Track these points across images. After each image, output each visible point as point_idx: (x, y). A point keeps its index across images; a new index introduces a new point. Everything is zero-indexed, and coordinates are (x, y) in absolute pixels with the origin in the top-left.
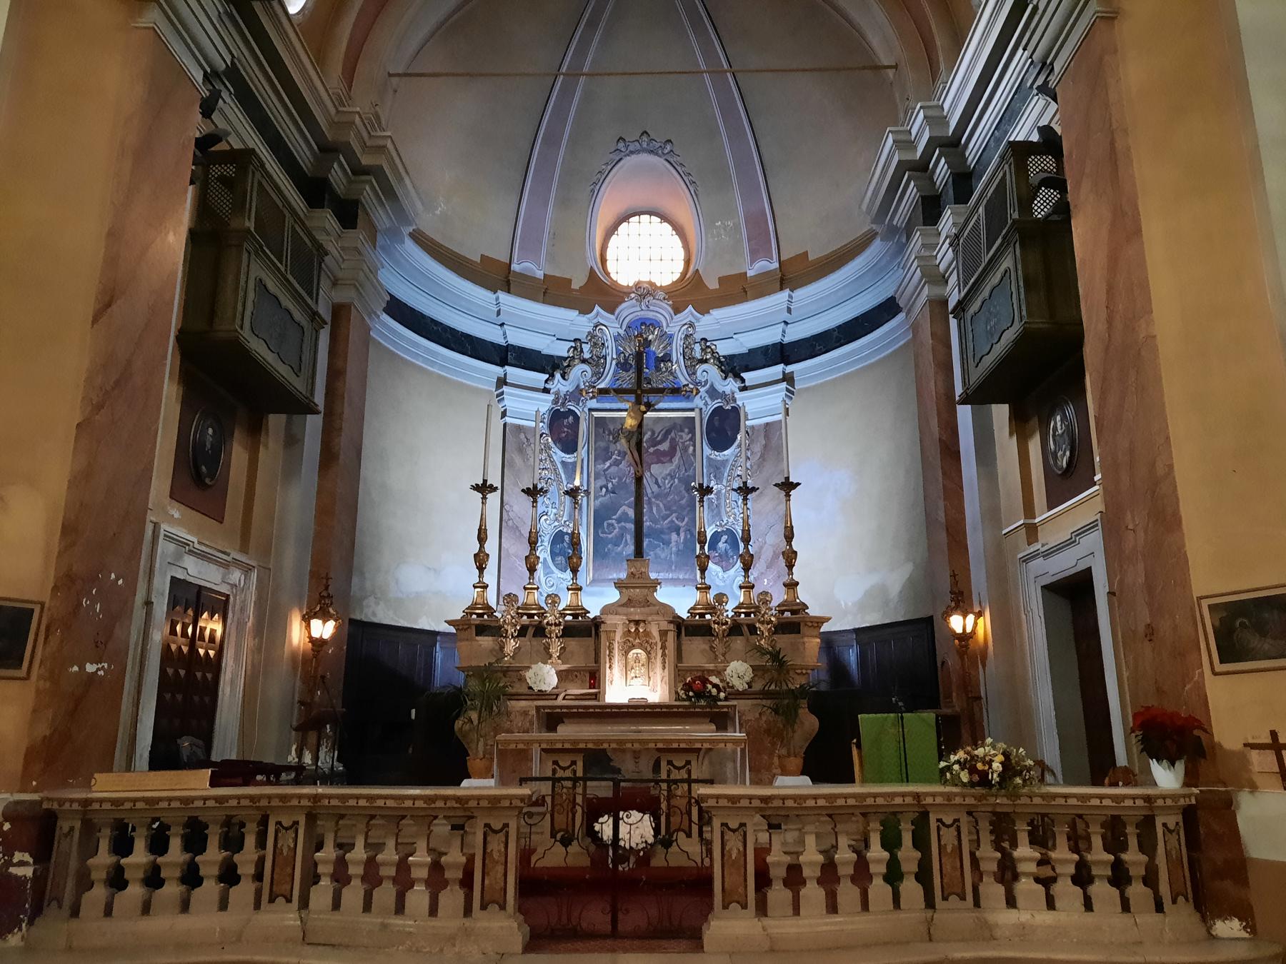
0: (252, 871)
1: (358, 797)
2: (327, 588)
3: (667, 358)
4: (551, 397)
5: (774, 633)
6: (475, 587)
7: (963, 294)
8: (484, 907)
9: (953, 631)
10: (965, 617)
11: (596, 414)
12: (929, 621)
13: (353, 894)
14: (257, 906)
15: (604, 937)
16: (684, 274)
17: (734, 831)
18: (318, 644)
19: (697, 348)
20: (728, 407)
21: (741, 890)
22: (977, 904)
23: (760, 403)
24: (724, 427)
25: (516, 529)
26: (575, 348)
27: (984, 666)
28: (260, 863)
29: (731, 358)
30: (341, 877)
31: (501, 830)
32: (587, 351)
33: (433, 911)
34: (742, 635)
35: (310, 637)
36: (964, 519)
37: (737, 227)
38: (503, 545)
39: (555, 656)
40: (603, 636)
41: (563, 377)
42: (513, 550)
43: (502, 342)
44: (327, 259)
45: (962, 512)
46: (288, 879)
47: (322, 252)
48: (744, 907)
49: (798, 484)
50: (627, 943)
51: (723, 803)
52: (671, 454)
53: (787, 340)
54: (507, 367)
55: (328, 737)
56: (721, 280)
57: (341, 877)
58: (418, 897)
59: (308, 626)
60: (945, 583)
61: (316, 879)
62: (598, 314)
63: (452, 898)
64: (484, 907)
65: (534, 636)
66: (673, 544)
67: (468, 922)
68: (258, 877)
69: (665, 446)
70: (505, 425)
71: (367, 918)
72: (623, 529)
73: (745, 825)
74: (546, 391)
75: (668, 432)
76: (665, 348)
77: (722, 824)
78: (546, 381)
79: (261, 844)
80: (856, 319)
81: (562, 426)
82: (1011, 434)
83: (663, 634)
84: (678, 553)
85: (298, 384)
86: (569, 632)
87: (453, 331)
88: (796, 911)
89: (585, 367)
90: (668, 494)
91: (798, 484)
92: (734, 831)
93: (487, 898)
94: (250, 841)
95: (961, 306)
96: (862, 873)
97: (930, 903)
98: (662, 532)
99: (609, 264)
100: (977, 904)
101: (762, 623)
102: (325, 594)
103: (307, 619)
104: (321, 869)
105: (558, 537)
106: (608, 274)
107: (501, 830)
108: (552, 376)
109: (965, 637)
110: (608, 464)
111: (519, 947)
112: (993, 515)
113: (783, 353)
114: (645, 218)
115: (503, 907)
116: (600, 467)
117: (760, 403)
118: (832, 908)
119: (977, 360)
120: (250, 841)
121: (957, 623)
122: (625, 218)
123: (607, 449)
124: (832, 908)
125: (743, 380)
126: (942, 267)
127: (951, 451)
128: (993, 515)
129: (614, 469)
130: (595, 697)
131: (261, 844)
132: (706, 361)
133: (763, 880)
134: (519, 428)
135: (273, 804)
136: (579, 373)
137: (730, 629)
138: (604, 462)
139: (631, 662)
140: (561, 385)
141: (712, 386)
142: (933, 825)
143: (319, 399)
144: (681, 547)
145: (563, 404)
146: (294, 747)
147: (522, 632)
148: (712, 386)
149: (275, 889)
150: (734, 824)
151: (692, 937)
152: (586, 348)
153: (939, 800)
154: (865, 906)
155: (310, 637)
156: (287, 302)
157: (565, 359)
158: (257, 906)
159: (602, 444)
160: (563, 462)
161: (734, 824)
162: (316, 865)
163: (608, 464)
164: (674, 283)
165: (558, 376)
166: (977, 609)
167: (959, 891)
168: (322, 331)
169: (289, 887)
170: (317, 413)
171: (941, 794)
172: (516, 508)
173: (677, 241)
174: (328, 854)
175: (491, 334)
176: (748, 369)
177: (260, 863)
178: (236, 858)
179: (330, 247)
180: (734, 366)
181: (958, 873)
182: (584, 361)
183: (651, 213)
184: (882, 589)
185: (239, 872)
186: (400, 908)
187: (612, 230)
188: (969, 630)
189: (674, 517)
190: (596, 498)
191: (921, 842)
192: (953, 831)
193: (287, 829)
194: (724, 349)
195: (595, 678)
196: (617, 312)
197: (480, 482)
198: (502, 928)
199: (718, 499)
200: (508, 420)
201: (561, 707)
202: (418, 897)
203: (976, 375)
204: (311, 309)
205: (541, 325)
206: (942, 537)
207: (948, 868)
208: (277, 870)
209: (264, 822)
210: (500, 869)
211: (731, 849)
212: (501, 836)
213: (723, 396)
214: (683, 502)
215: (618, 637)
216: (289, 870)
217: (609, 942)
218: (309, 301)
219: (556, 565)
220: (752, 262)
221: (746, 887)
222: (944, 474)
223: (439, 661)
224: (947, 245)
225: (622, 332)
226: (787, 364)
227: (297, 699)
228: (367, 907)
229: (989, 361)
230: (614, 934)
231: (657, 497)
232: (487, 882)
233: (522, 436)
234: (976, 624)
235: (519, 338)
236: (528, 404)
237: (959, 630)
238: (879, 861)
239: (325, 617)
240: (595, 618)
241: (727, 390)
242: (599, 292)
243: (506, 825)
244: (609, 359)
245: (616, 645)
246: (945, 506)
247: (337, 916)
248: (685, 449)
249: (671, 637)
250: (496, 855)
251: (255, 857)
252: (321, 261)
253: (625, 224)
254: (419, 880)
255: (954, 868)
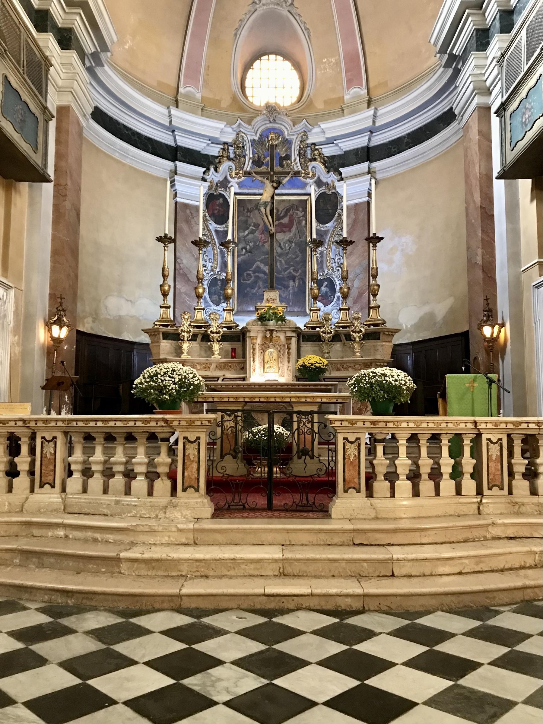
0: (27, 468)
1: (96, 420)
2: (61, 304)
3: (288, 157)
4: (207, 184)
5: (362, 340)
6: (161, 307)
7: (505, 98)
8: (184, 490)
9: (485, 336)
10: (493, 327)
11: (239, 197)
12: (466, 335)
13: (96, 482)
14: (32, 491)
15: (263, 510)
16: (300, 99)
17: (352, 443)
18: (57, 341)
19: (309, 151)
20: (330, 193)
21: (356, 480)
22: (510, 493)
23: (351, 188)
24: (328, 204)
25: (185, 275)
26: (224, 149)
27: (503, 361)
28: (32, 463)
29: (332, 158)
30: (87, 473)
31: (195, 442)
32: (233, 151)
33: (150, 493)
34: (341, 341)
35: (52, 337)
36: (494, 262)
37: (338, 63)
38: (177, 286)
39: (216, 353)
40: (248, 342)
41: (216, 171)
42: (183, 290)
43: (173, 144)
44: (51, 69)
45: (493, 257)
46: (52, 473)
47: (48, 64)
48: (358, 491)
49: (382, 238)
50: (279, 514)
51: (345, 424)
52: (289, 227)
53: (372, 144)
54: (177, 163)
55: (67, 404)
56: (326, 102)
57: (87, 473)
58: (140, 484)
59: (50, 330)
60: (480, 302)
61: (70, 474)
62: (240, 124)
63: (162, 485)
64: (184, 490)
65: (202, 341)
66: (291, 288)
67: (174, 500)
68: (31, 473)
69: (285, 221)
70: (176, 203)
71: (105, 497)
72: (257, 278)
73: (359, 439)
74: (204, 180)
75: (288, 210)
76: (286, 150)
77: (344, 439)
78: (204, 173)
79: (32, 451)
80: (420, 128)
81: (216, 205)
82: (532, 200)
83: (289, 339)
84: (294, 294)
85: (36, 159)
86: (224, 338)
87: (139, 135)
88: (393, 495)
89: (231, 163)
90: (288, 254)
91: (382, 238)
92: (352, 443)
93: (186, 484)
94: (24, 449)
95: (503, 107)
96: (435, 475)
97: (480, 492)
98: (283, 279)
99: (247, 90)
100: (510, 493)
101: (355, 332)
102: (60, 308)
103: (48, 325)
104: (73, 467)
105: (213, 282)
106: (246, 97)
107: (195, 442)
108: (208, 169)
109: (494, 340)
110: (246, 232)
111: (209, 516)
112: (514, 257)
113: (368, 154)
114: (272, 57)
115: (197, 490)
116: (241, 234)
117: (351, 188)
118: (416, 493)
119: (513, 145)
120: (24, 449)
121: (487, 331)
122: (257, 56)
123: (246, 222)
124: (416, 493)
125: (340, 174)
126: (488, 83)
127: (487, 216)
128: (514, 257)
129: (251, 236)
130: (244, 379)
131: (32, 451)
132: (315, 160)
133: (371, 478)
134: (186, 206)
135: (38, 425)
136: (225, 165)
137: (333, 337)
138: (244, 231)
139: (267, 358)
140: (214, 177)
141: (319, 178)
142: (484, 442)
143: (51, 171)
144: (296, 290)
145: (216, 190)
146: (45, 409)
147: (194, 338)
148: (319, 178)
149: (43, 479)
150: (352, 438)
151: (324, 512)
152: (231, 149)
153: (489, 426)
154: (437, 493)
155: (52, 337)
156: (25, 96)
157: (217, 157)
158: (32, 491)
159: (243, 218)
160: (216, 231)
161: (352, 438)
162: (69, 465)
163: (246, 232)
164: (292, 105)
165: (212, 169)
166: (500, 322)
167: (499, 484)
168: (51, 122)
169: (51, 478)
170: (49, 181)
171: (491, 422)
172: (185, 261)
173: (294, 74)
174: (78, 455)
175: (166, 138)
176: (344, 166)
177: (32, 463)
178: (16, 459)
179: (53, 62)
180: (335, 164)
181: (500, 472)
182: (229, 159)
183: (276, 54)
184: (431, 316)
185: (18, 469)
186: (128, 492)
187: (248, 66)
188: (495, 335)
189: (291, 270)
190: (238, 256)
191: (476, 452)
192: (497, 446)
193: (49, 441)
194: (328, 151)
195: (243, 368)
196: (253, 124)
197: (163, 235)
198: (197, 503)
199: (322, 257)
200: (178, 199)
201: (221, 385)
202: (140, 484)
203: (511, 157)
204: (42, 105)
205: (202, 130)
206: (479, 274)
207: (492, 470)
208: (43, 467)
209: (33, 437)
210: (195, 466)
211: (349, 456)
212: (195, 445)
213: (327, 184)
214: (298, 259)
215: (259, 341)
216: (52, 467)
217: (267, 513)
218: (40, 98)
219: (212, 301)
220: (348, 89)
221: (359, 478)
222: (483, 231)
223: (136, 362)
224: (494, 63)
225: (256, 138)
226: (371, 161)
227: (45, 378)
228: (105, 491)
229: (522, 145)
230: (270, 507)
231: (280, 255)
232: (186, 474)
233: (188, 211)
234: (500, 331)
235: (184, 142)
236: (193, 188)
237: (488, 335)
238: (446, 465)
239: (59, 323)
240: (243, 328)
241: (329, 181)
242: (239, 107)
243: (198, 438)
244: (247, 158)
245: (257, 347)
246: (483, 253)
247: (85, 496)
248: (300, 223)
249: (294, 341)
250: (191, 457)
251: (29, 459)
252: (47, 70)
253: (258, 62)
254: (140, 473)
255: (497, 469)
